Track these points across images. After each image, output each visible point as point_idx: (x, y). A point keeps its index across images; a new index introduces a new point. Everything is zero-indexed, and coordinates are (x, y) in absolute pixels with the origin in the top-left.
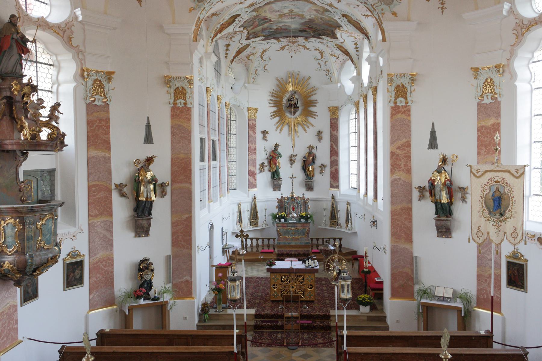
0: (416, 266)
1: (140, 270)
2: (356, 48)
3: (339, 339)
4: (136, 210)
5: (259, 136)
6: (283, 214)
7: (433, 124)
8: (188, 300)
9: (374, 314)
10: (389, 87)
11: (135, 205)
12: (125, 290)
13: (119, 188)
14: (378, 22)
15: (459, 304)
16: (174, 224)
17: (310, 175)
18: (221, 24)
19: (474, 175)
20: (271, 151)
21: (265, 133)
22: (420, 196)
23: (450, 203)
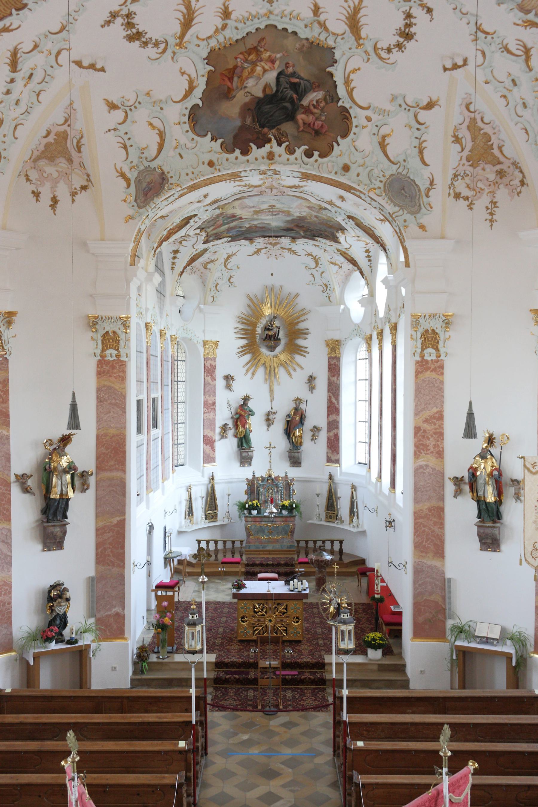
0: (450, 592)
1: (51, 599)
2: (368, 256)
3: (337, 702)
4: (45, 511)
5: (220, 383)
6: (255, 502)
7: (470, 403)
8: (119, 642)
9: (388, 661)
10: (414, 333)
11: (45, 505)
12: (27, 629)
13: (21, 481)
14: (399, 237)
15: (509, 648)
16: (99, 532)
17: (297, 442)
18: (168, 229)
19: (529, 470)
20: (238, 405)
21: (228, 378)
22: (456, 491)
23: (499, 503)
